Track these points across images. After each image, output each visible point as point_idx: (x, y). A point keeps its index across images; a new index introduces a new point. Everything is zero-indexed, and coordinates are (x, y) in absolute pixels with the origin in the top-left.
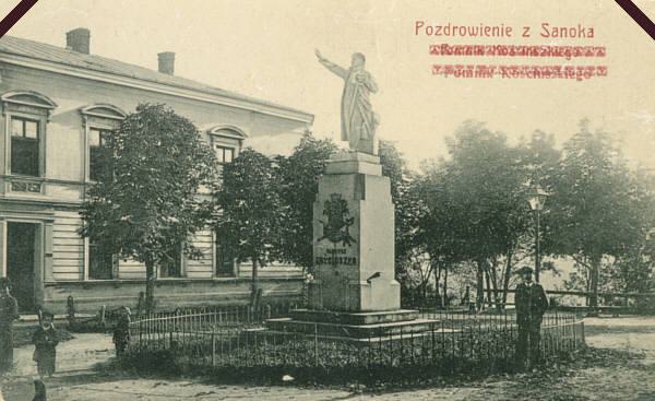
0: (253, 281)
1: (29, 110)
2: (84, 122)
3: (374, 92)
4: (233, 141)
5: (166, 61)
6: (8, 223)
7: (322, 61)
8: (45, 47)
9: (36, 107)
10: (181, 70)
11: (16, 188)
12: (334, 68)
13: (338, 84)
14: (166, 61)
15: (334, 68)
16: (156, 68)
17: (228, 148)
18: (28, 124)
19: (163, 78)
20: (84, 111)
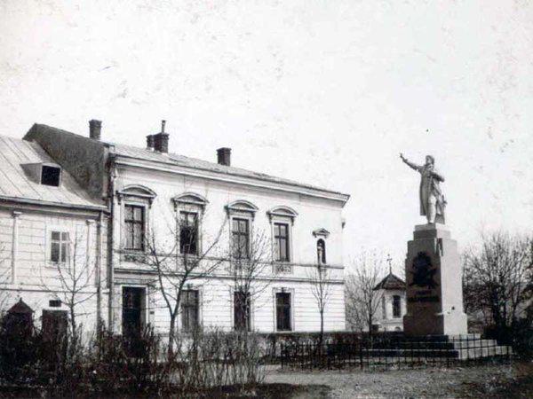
0: (468, 348)
1: (137, 199)
2: (175, 206)
3: (443, 181)
4: (287, 219)
5: (95, 126)
6: (126, 290)
7: (405, 161)
8: (133, 149)
9: (286, 216)
10: (104, 137)
11: (127, 259)
12: (414, 167)
13: (416, 177)
14: (95, 126)
15: (414, 167)
16: (214, 159)
17: (283, 224)
18: (241, 222)
19: (222, 168)
20: (120, 192)
